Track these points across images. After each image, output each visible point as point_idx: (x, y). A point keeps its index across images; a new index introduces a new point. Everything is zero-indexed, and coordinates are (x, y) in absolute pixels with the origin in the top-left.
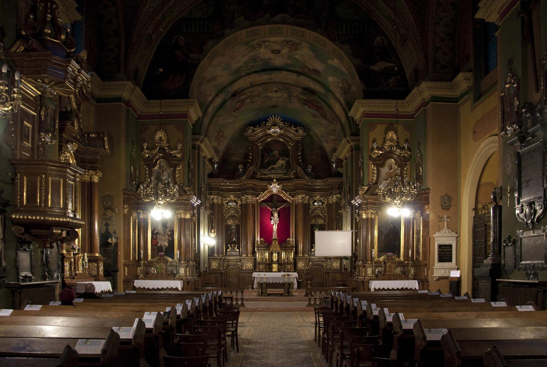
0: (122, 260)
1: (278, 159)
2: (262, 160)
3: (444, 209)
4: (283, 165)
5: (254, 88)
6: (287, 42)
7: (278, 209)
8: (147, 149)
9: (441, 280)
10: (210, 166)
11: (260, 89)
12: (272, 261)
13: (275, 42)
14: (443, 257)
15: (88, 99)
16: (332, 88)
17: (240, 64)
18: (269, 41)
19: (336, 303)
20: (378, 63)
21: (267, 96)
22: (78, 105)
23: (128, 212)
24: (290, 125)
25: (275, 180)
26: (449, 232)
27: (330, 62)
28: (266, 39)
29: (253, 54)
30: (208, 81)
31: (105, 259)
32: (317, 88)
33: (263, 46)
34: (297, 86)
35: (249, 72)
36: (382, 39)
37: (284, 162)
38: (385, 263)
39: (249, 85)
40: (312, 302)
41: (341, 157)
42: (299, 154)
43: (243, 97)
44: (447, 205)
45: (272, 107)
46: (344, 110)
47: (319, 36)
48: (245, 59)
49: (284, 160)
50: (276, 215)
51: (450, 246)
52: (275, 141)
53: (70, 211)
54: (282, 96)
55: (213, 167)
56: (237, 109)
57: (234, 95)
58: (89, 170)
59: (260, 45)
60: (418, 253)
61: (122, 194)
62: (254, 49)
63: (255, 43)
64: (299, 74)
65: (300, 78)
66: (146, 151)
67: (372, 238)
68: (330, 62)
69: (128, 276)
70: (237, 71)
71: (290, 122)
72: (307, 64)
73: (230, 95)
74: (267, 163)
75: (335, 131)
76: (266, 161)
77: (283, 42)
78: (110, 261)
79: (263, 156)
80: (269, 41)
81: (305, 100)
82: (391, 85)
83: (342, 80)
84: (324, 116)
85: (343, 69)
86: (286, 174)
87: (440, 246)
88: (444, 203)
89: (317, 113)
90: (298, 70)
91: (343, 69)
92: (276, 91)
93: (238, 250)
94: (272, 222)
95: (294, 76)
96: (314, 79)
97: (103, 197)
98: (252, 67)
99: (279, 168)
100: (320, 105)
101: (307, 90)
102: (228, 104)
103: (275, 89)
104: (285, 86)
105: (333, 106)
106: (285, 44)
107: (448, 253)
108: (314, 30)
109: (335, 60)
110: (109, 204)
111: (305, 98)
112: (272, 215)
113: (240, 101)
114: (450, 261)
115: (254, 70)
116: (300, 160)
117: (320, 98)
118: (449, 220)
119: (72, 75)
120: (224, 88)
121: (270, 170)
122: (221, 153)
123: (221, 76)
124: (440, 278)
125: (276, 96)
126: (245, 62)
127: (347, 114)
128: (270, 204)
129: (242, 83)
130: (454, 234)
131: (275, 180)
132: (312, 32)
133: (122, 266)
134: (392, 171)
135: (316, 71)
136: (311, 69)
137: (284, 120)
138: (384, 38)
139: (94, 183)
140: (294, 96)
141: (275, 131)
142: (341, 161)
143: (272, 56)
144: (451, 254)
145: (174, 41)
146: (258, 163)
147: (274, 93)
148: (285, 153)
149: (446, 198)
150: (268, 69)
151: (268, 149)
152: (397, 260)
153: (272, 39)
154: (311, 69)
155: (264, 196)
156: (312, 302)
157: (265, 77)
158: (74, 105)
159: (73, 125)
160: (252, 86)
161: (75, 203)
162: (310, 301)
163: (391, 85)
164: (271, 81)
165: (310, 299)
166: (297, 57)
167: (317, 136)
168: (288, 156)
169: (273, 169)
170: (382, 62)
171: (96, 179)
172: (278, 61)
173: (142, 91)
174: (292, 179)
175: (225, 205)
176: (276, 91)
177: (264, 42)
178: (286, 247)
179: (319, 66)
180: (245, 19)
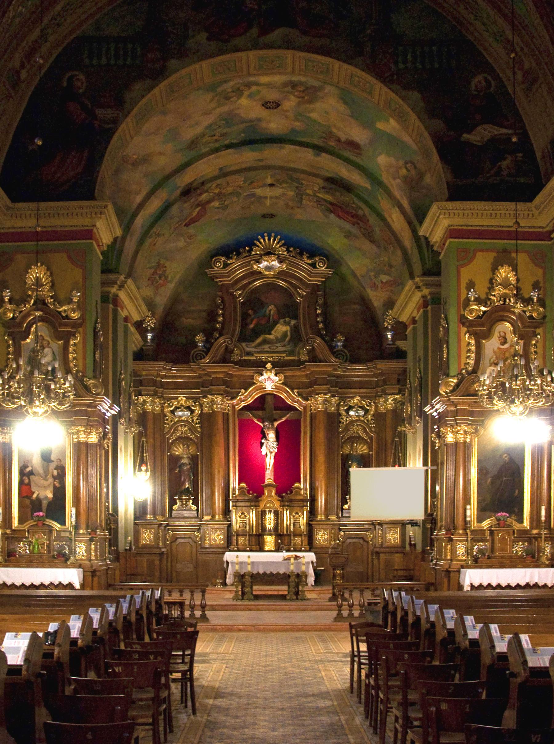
1: (276, 323)
2: (244, 325)
4: (285, 335)
5: (228, 178)
6: (294, 85)
7: (276, 424)
8: (11, 301)
10: (138, 336)
11: (240, 180)
12: (264, 529)
16: (385, 178)
17: (199, 130)
18: (257, 84)
19: (394, 614)
20: (479, 128)
21: (253, 195)
24: (301, 254)
25: (269, 366)
27: (380, 125)
28: (252, 79)
29: (225, 109)
30: (133, 164)
32: (355, 178)
33: (246, 93)
35: (217, 145)
36: (486, 79)
37: (288, 328)
38: (492, 533)
39: (217, 173)
40: (345, 613)
42: (319, 311)
43: (204, 196)
45: (264, 216)
46: (410, 223)
47: (359, 72)
49: (288, 324)
50: (271, 435)
52: (270, 287)
55: (145, 338)
56: (193, 221)
57: (187, 192)
59: (238, 92)
62: (227, 98)
63: (228, 86)
64: (318, 149)
65: (319, 159)
68: (380, 125)
70: (193, 144)
71: (300, 248)
72: (334, 130)
73: (179, 192)
74: (253, 330)
75: (391, 266)
76: (252, 326)
77: (285, 85)
79: (245, 317)
81: (331, 204)
83: (406, 163)
84: (369, 236)
85: (406, 138)
86: (291, 353)
89: (354, 230)
90: (315, 141)
91: (406, 138)
92: (271, 185)
94: (264, 450)
95: (308, 155)
96: (347, 161)
98: (224, 135)
99: (278, 340)
100: (360, 212)
101: (335, 183)
102: (175, 210)
103: (269, 181)
104: (289, 175)
105: (386, 216)
106: (289, 88)
108: (349, 60)
109: (392, 121)
111: (329, 198)
112: (264, 436)
113: (198, 205)
115: (227, 142)
116: (321, 325)
120: (167, 178)
121: (260, 344)
122: (160, 310)
123: (160, 154)
126: (209, 127)
127: (414, 232)
128: (260, 413)
129: (204, 168)
131: (269, 366)
132: (345, 66)
134: (506, 346)
135: (353, 145)
137: (288, 244)
140: (308, 195)
141: (269, 265)
143: (264, 113)
146: (234, 331)
147: (268, 189)
148: (289, 310)
150: (256, 139)
151: (254, 301)
152: (517, 526)
153: (264, 79)
154: (343, 140)
155: (247, 397)
156: (345, 613)
157: (248, 156)
160: (224, 174)
162: (340, 611)
163: (505, 173)
164: (261, 164)
165: (340, 607)
166: (313, 115)
168: (296, 317)
169: (265, 342)
170: (486, 126)
172: (275, 125)
174: (303, 363)
176: (271, 185)
177: (248, 85)
178: (291, 501)
179: (359, 135)
180: (208, 39)
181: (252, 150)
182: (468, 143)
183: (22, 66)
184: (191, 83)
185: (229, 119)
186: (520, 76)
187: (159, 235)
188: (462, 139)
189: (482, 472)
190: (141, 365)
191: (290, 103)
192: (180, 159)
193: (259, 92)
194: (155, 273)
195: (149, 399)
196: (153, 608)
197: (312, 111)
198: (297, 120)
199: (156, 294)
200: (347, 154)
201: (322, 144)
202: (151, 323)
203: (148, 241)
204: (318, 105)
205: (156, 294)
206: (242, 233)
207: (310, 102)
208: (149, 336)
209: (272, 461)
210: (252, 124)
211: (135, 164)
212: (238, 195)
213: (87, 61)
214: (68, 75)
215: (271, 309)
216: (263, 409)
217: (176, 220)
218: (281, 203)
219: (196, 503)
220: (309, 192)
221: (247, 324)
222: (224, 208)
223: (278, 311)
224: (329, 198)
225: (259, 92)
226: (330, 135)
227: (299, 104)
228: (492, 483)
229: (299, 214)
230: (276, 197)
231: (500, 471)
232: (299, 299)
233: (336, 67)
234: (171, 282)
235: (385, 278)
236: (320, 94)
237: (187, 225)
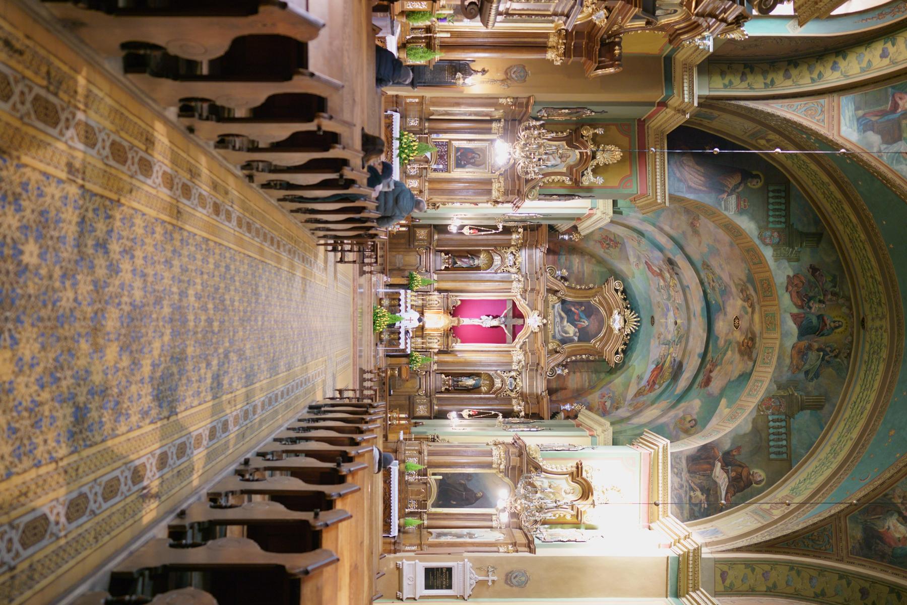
0: (429, 93)
1: (575, 326)
2: (574, 304)
3: (507, 575)
4: (566, 332)
5: (681, 292)
7: (503, 326)
8: (595, 135)
9: (397, 572)
11: (680, 299)
13: (752, 319)
14: (433, 575)
15: (670, 42)
16: (683, 405)
17: (718, 271)
18: (753, 313)
19: (366, 413)
20: (725, 475)
21: (668, 310)
22: (662, 28)
23: (501, 105)
24: (625, 344)
25: (545, 321)
26: (471, 585)
28: (757, 307)
29: (734, 290)
31: (431, 67)
32: (683, 383)
33: (746, 304)
34: (684, 355)
35: (706, 284)
36: (761, 481)
37: (572, 335)
39: (685, 283)
41: (581, 417)
43: (667, 275)
44: (514, 581)
45: (653, 317)
46: (650, 422)
48: (726, 278)
49: (575, 335)
50: (495, 323)
51: (450, 587)
52: (601, 322)
53: (508, 6)
54: (669, 332)
55: (563, 234)
56: (649, 268)
57: (671, 262)
58: (565, 44)
59: (747, 299)
60: (439, 535)
61: (527, 95)
62: (742, 291)
64: (704, 356)
65: (696, 357)
66: (591, 132)
67: (463, 465)
69: (406, 103)
70: (706, 266)
71: (629, 344)
72: (718, 368)
73: (672, 257)
74: (571, 310)
76: (573, 309)
77: (753, 333)
78: (428, 76)
79: (580, 304)
80: (753, 313)
81: (663, 365)
82: (692, 494)
83: (695, 420)
86: (554, 337)
87: (449, 570)
88: (516, 576)
89: (644, 383)
92: (676, 323)
93: (443, 268)
94: (484, 317)
95: (700, 349)
97: (524, 67)
100: (657, 386)
101: (678, 369)
102: (658, 254)
105: (655, 405)
106: (749, 335)
107: (439, 582)
110: (514, 76)
111: (667, 364)
112: (494, 317)
113: (661, 270)
114: (428, 587)
116: (574, 358)
117: (668, 387)
118: (490, 583)
119: (718, 8)
120: (682, 248)
123: (700, 243)
124: (399, 569)
125: (668, 324)
126: (721, 278)
127: (645, 425)
128: (511, 314)
129: (688, 274)
130: (468, 592)
131: (545, 321)
133: (421, 94)
135: (708, 381)
136: (712, 374)
137: (633, 335)
138: (763, 483)
139: (545, 52)
140: (669, 349)
141: (617, 322)
142: (576, 417)
144: (438, 588)
145: (754, 173)
147: (673, 321)
148: (584, 336)
149: (523, 579)
151: (590, 311)
153: (757, 317)
154: (712, 374)
155: (522, 306)
157: (697, 306)
158: (664, 21)
159: (636, 17)
160: (684, 289)
161: (520, 15)
163: (692, 494)
166: (729, 353)
167: (610, 382)
168: (580, 340)
169: (562, 318)
170: (727, 480)
171: (550, 55)
172: (722, 326)
173: (680, 126)
174: (547, 345)
175: (509, 251)
176: (676, 323)
177: (752, 306)
178: (448, 337)
180: (788, 277)
181: (702, 309)
182: (714, 465)
183: (768, 141)
184: (754, 264)
185: (725, 292)
186: (767, 507)
187: (639, 243)
188: (716, 462)
189: (469, 475)
190: (545, 230)
191: (738, 336)
192: (696, 257)
193: (747, 313)
194: (611, 240)
195: (520, 236)
196: (372, 232)
197: (733, 352)
198: (726, 341)
199: (596, 241)
200: (700, 379)
201: (708, 359)
202: (575, 237)
203: (635, 235)
204: (737, 356)
205: (596, 241)
206: (641, 302)
207: (740, 351)
208: (566, 237)
209: (477, 324)
210: (721, 309)
211: (692, 225)
212: (669, 299)
213: (771, 188)
214: (761, 175)
215: (585, 323)
216: (514, 317)
217: (650, 255)
218: (662, 330)
219: (447, 269)
220: (671, 350)
221: (574, 306)
222: (658, 290)
223: (585, 328)
224: (667, 364)
225: (747, 313)
226: (714, 365)
227: (738, 343)
228: (461, 484)
229: (654, 343)
230: (667, 327)
231: (470, 490)
232: (593, 341)
233: (769, 370)
234: (605, 252)
235: (608, 404)
236: (746, 357)
237: (646, 263)
